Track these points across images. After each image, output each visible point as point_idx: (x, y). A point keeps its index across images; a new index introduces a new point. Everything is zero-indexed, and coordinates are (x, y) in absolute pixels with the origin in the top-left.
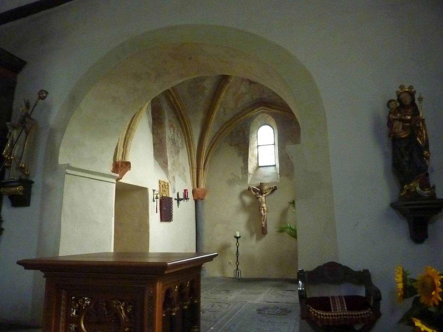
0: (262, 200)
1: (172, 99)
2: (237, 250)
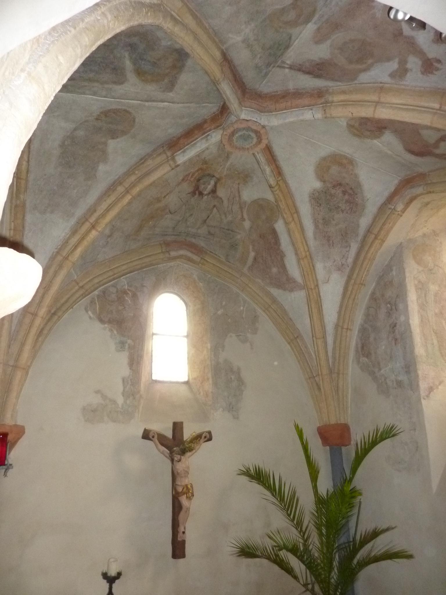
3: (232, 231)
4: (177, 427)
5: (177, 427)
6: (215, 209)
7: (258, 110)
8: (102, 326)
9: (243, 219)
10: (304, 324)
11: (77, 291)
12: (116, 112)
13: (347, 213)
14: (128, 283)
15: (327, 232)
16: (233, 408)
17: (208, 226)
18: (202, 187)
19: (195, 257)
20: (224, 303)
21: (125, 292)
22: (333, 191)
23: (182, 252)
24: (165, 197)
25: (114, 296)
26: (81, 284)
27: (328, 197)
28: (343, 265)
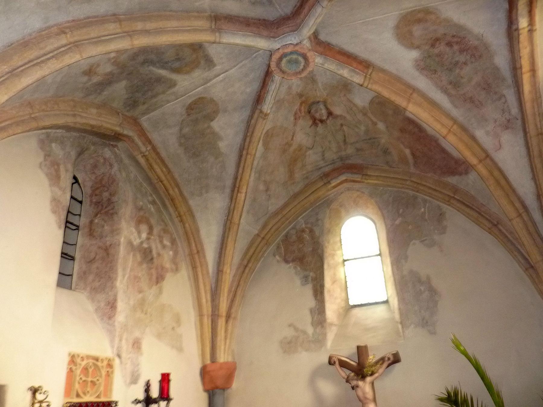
0: (364, 393)
1: (142, 161)
3: (374, 138)
4: (361, 351)
5: (361, 351)
7: (291, 31)
10: (501, 206)
12: (195, 103)
13: (472, 62)
15: (464, 94)
16: (427, 322)
18: (317, 116)
20: (401, 211)
21: (303, 231)
22: (436, 51)
23: (343, 178)
24: (292, 139)
26: (262, 236)
27: (437, 59)
28: (509, 121)
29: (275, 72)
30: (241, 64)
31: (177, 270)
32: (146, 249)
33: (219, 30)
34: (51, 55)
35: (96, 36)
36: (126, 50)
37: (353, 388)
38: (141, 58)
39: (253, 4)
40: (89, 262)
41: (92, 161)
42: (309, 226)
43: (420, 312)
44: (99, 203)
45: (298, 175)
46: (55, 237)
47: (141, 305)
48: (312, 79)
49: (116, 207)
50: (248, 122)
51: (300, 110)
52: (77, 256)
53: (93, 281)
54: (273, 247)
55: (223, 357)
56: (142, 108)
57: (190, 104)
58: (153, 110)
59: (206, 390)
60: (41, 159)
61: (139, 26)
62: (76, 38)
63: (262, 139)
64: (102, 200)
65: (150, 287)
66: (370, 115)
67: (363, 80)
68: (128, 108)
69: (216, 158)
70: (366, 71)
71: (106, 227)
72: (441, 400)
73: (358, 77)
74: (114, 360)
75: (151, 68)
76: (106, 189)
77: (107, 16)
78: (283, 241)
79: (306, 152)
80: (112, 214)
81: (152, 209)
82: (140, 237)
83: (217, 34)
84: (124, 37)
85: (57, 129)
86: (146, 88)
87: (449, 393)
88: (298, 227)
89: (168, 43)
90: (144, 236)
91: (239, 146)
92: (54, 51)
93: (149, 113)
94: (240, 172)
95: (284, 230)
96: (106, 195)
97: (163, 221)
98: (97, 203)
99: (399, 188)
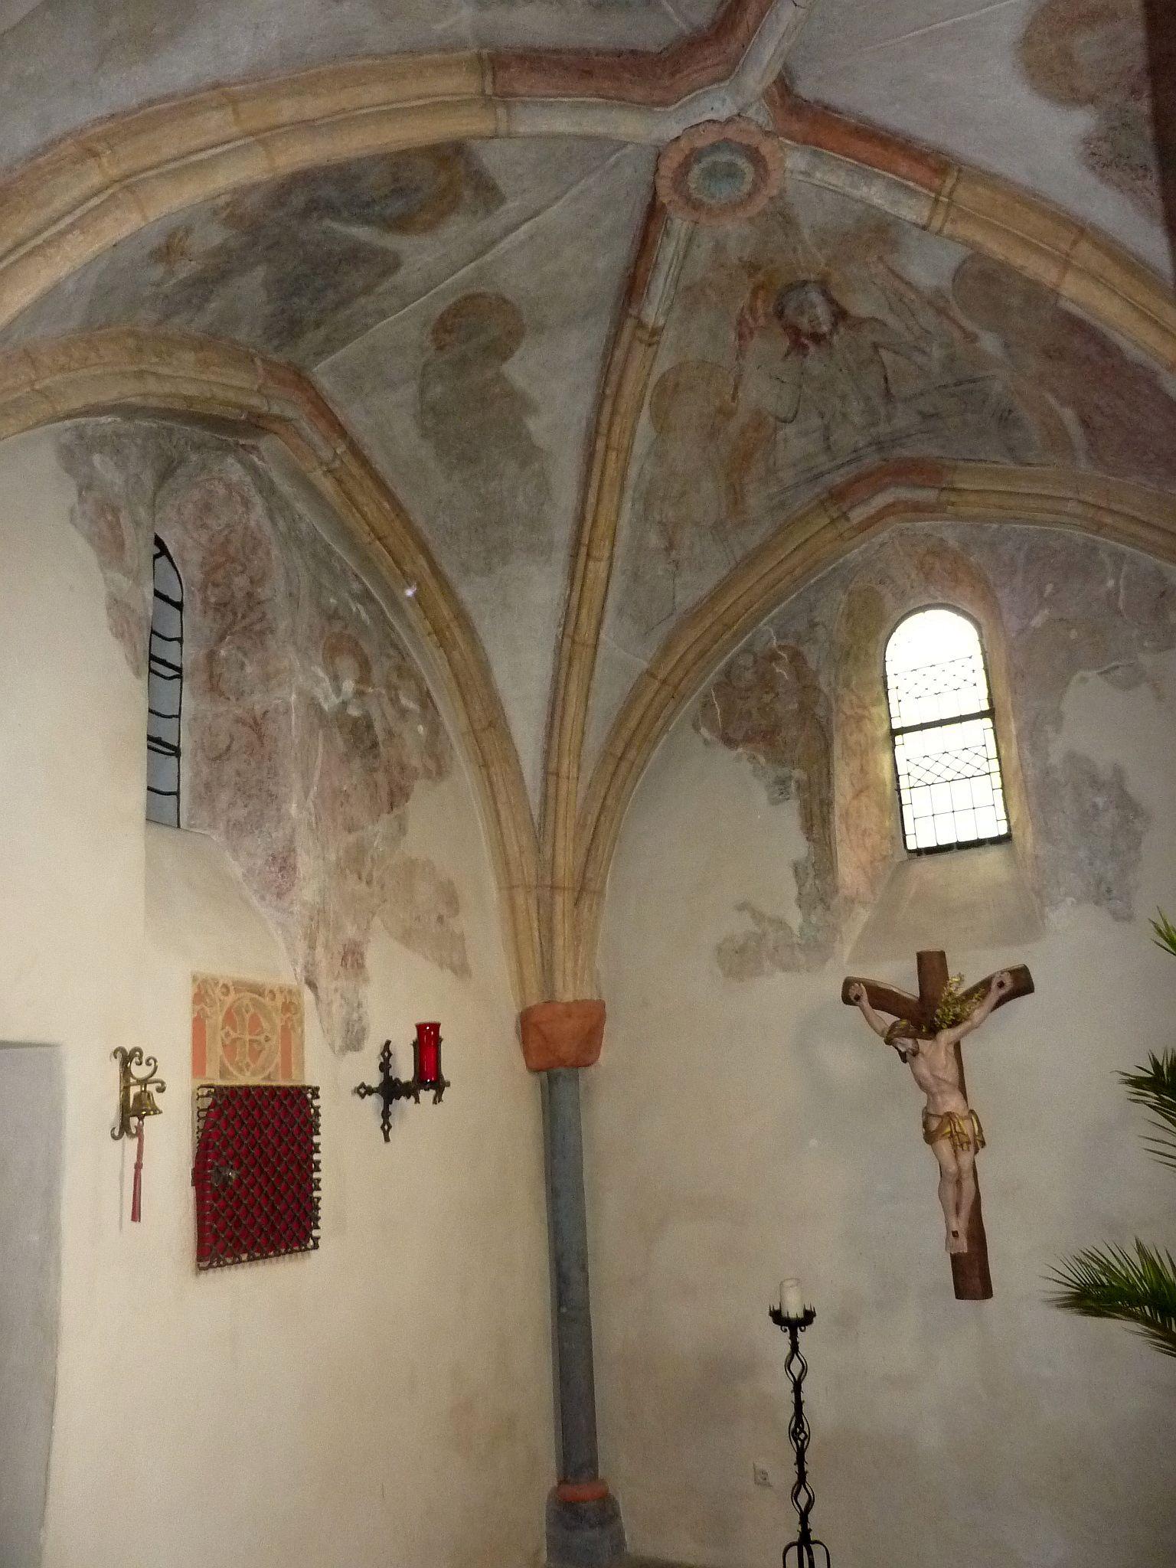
1: (327, 485)
2: (799, 1405)
3: (971, 381)
5: (931, 966)
6: (883, 353)
8: (734, 753)
9: (971, 338)
11: (657, 692)
14: (778, 634)
16: (1109, 891)
17: (905, 400)
18: (804, 323)
19: (928, 495)
20: (1049, 588)
21: (774, 657)
23: (880, 501)
24: (734, 397)
25: (749, 675)
26: (661, 677)
29: (670, 208)
30: (574, 191)
31: (439, 768)
32: (355, 721)
33: (502, 98)
34: (69, 220)
35: (174, 152)
36: (255, 186)
37: (903, 1057)
38: (298, 200)
39: (599, 7)
40: (214, 760)
41: (196, 494)
42: (791, 642)
43: (1091, 864)
44: (225, 605)
45: (755, 502)
46: (119, 698)
47: (356, 860)
48: (784, 218)
49: (269, 616)
50: (604, 356)
51: (752, 310)
52: (186, 745)
53: (232, 804)
54: (691, 705)
55: (568, 992)
56: (314, 338)
57: (441, 317)
58: (344, 343)
59: (534, 1070)
60: (73, 498)
61: (287, 109)
62: (125, 167)
63: (647, 400)
64: (233, 596)
65: (376, 818)
66: (956, 312)
67: (926, 213)
68: (276, 342)
69: (524, 464)
70: (937, 182)
71: (249, 669)
72: (1137, 1082)
73: (912, 202)
74: (299, 994)
75: (327, 222)
76: (240, 568)
77: (199, 90)
78: (718, 686)
79: (775, 430)
80: (262, 633)
81: (364, 615)
82: (338, 690)
83: (501, 112)
84: (247, 147)
85: (100, 414)
86: (319, 282)
87: (1156, 1066)
88: (758, 648)
89: (365, 153)
90: (349, 686)
91: (584, 423)
92: (75, 207)
93: (333, 351)
94: (592, 499)
95: (721, 659)
96: (241, 582)
97: (395, 646)
98: (222, 606)
99: (1043, 523)
